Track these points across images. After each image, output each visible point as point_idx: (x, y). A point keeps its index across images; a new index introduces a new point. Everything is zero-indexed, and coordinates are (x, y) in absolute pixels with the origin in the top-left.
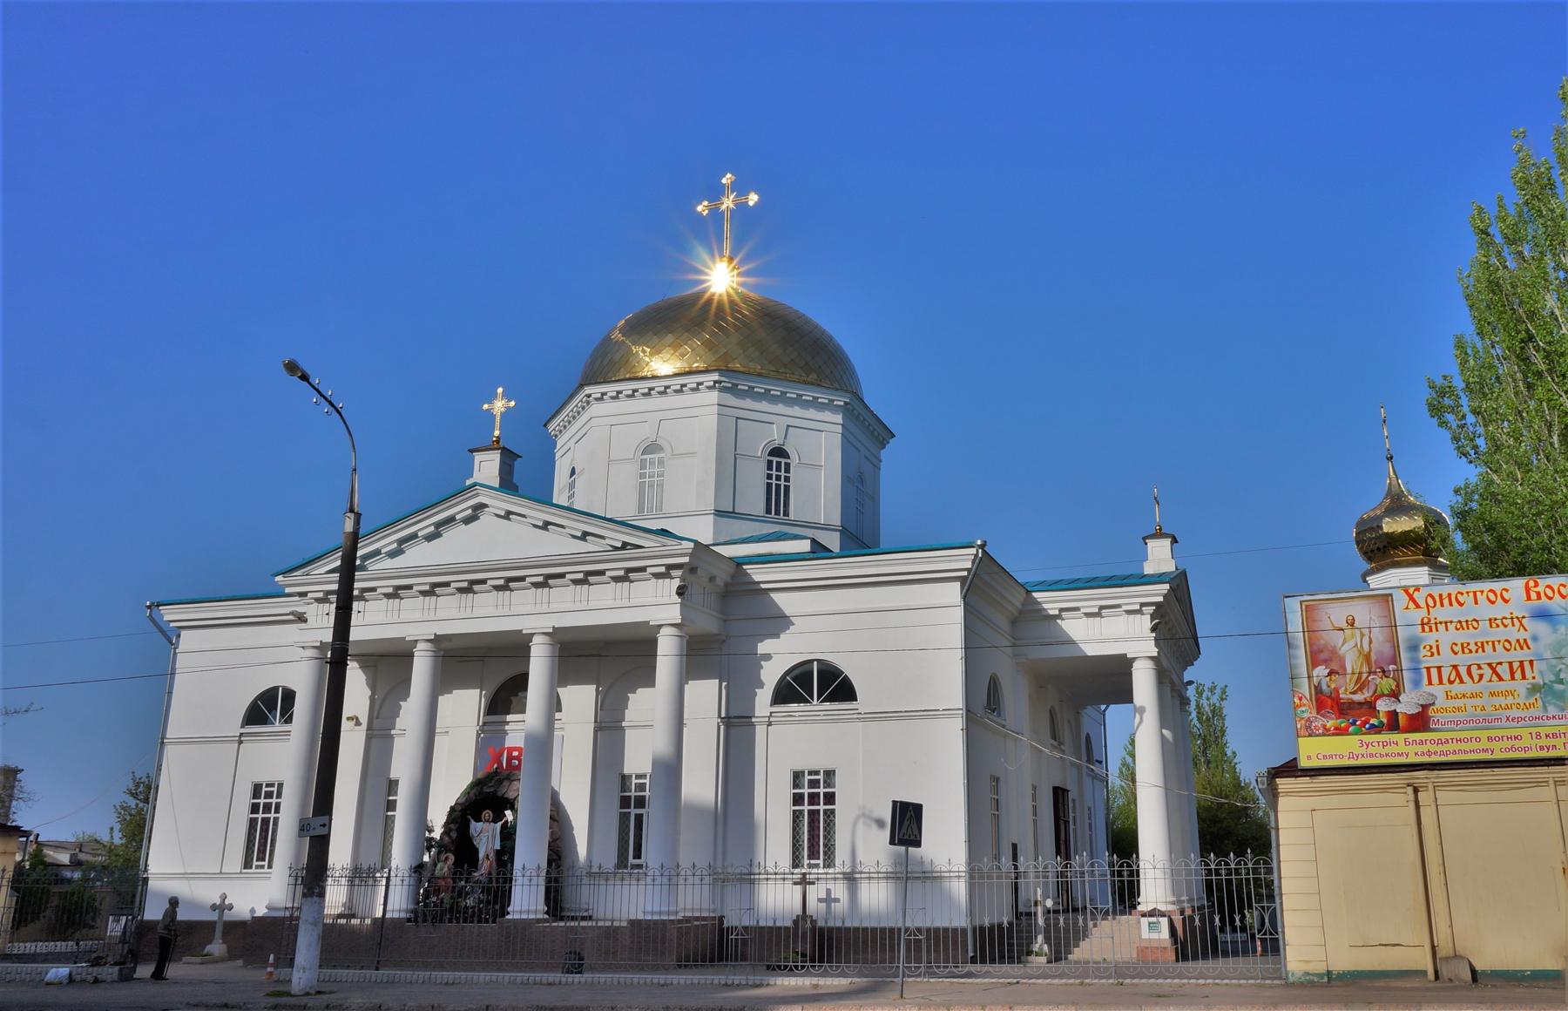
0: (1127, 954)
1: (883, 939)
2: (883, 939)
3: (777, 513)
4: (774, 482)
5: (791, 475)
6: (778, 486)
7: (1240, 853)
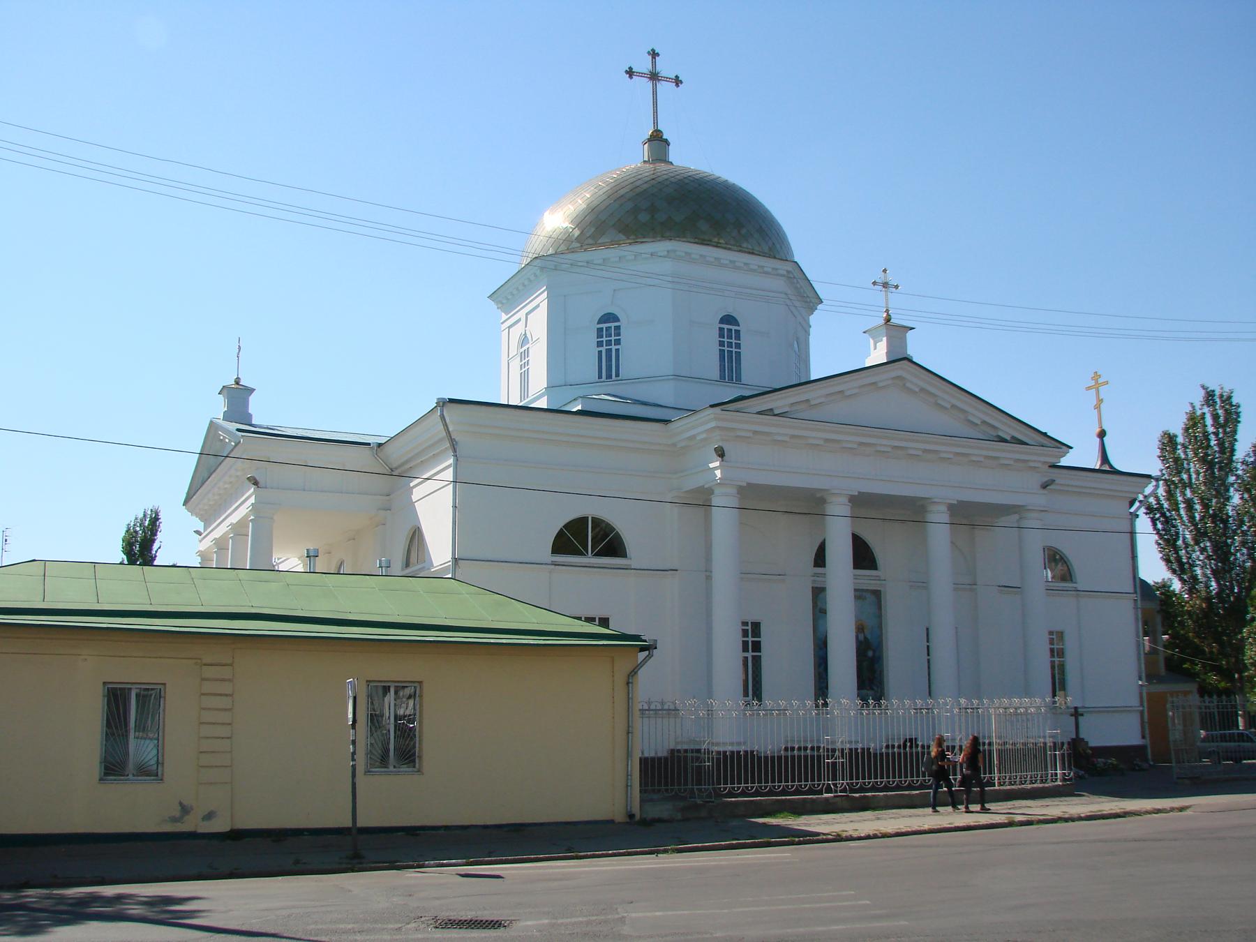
1: (653, 766)
2: (653, 766)
3: (609, 376)
5: (742, 342)
7: (1210, 696)
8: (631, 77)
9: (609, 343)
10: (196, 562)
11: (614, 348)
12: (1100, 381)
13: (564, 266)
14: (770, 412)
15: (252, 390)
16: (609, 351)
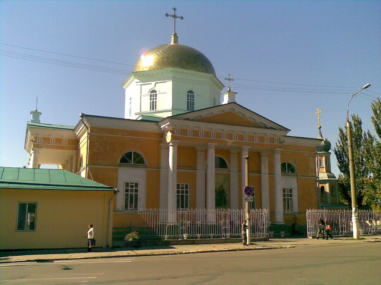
0: (256, 239)
4: (189, 101)
8: (182, 17)
9: (153, 99)
10: (23, 167)
13: (141, 76)
14: (188, 119)
15: (41, 113)
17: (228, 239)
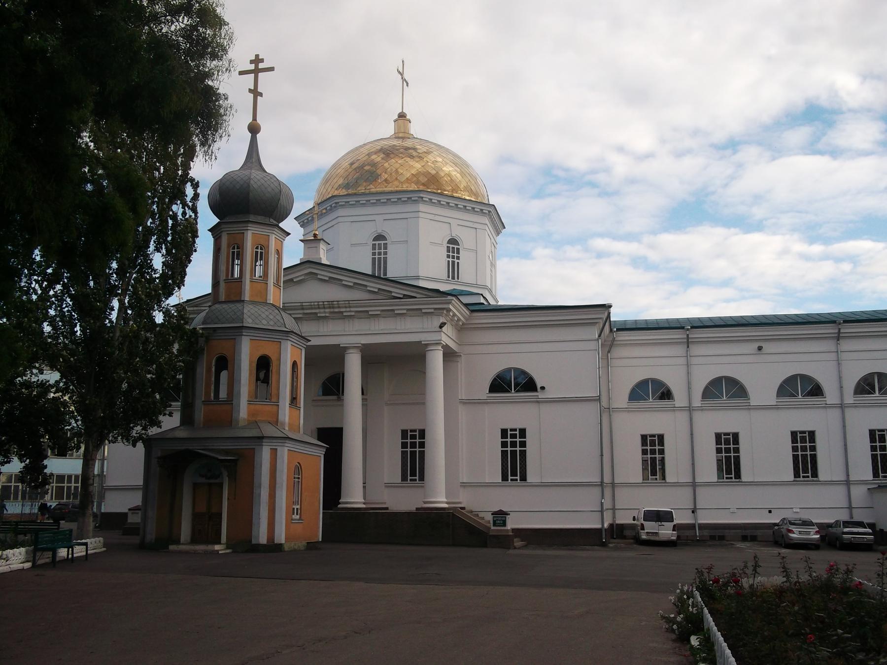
3: (453, 278)
6: (380, 259)
9: (380, 254)
11: (456, 261)
12: (261, 66)
16: (453, 262)
17: (187, 553)
